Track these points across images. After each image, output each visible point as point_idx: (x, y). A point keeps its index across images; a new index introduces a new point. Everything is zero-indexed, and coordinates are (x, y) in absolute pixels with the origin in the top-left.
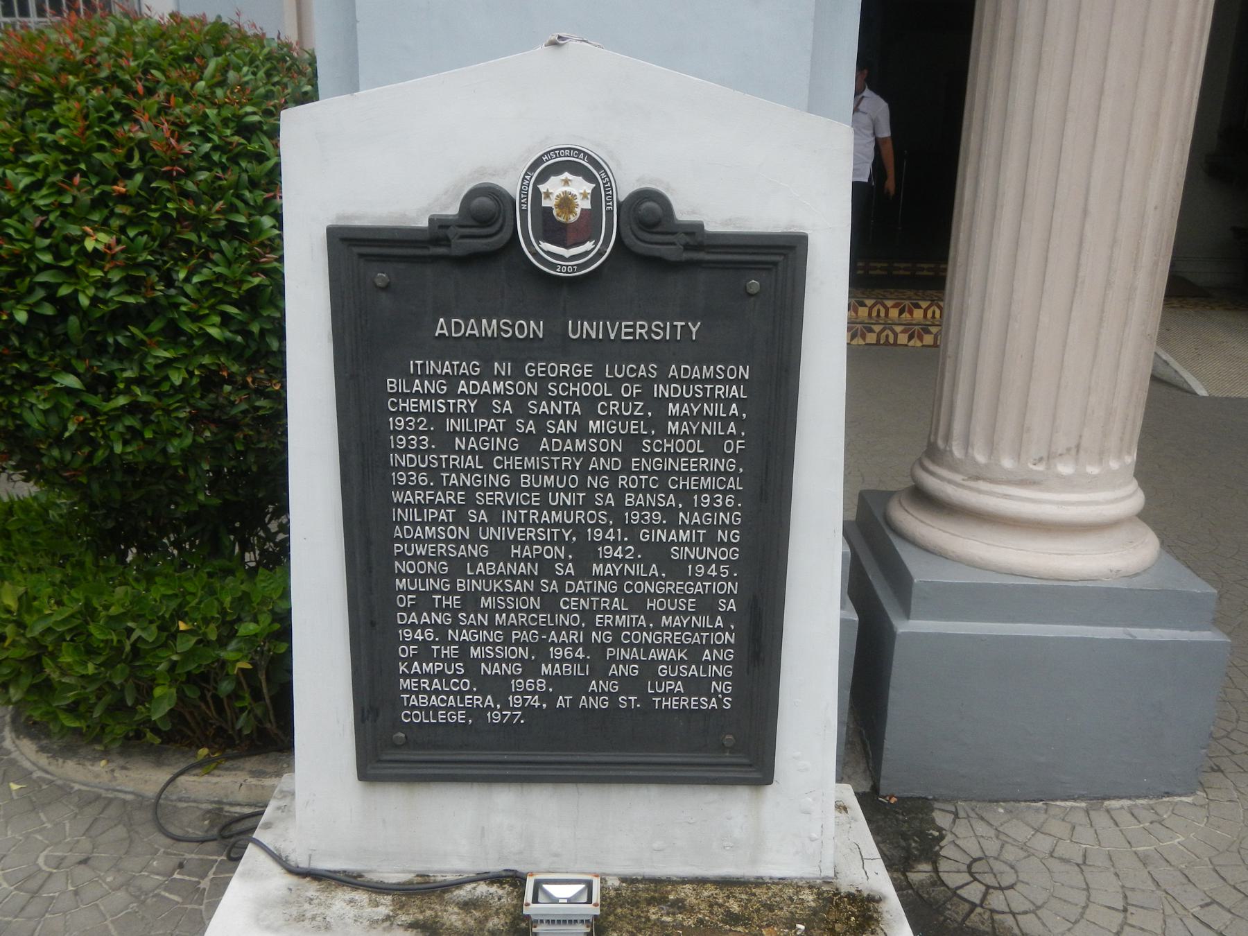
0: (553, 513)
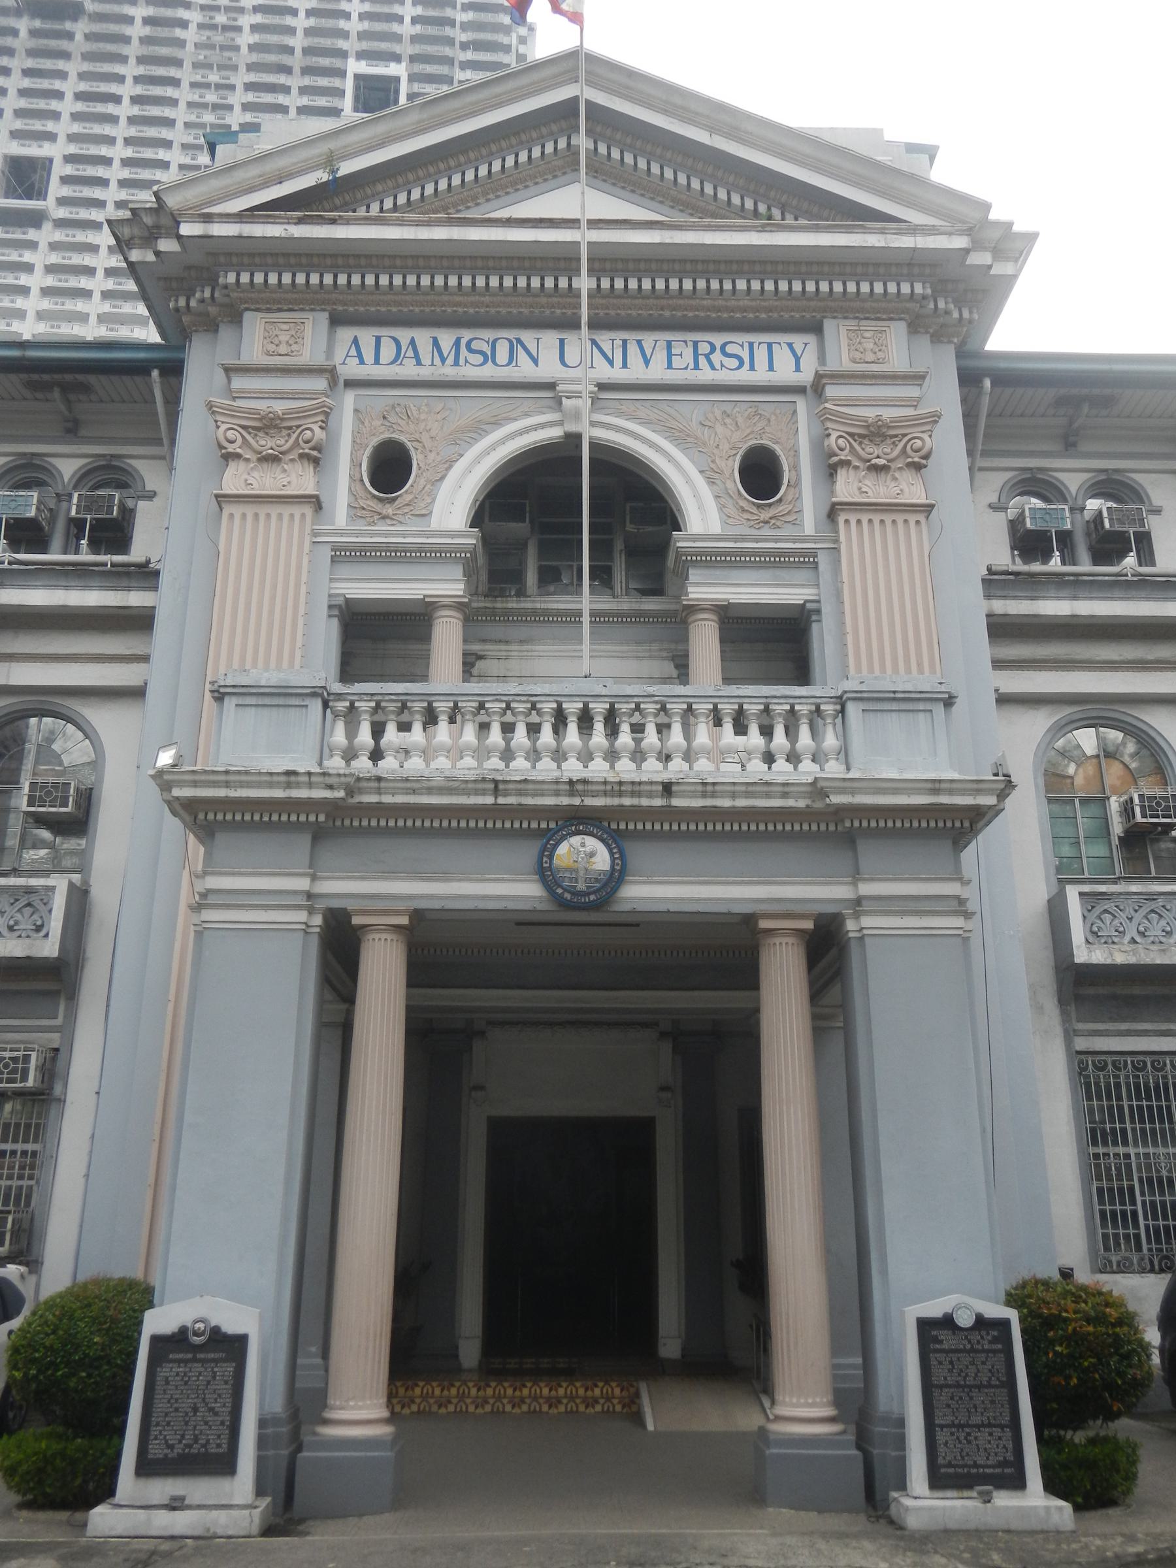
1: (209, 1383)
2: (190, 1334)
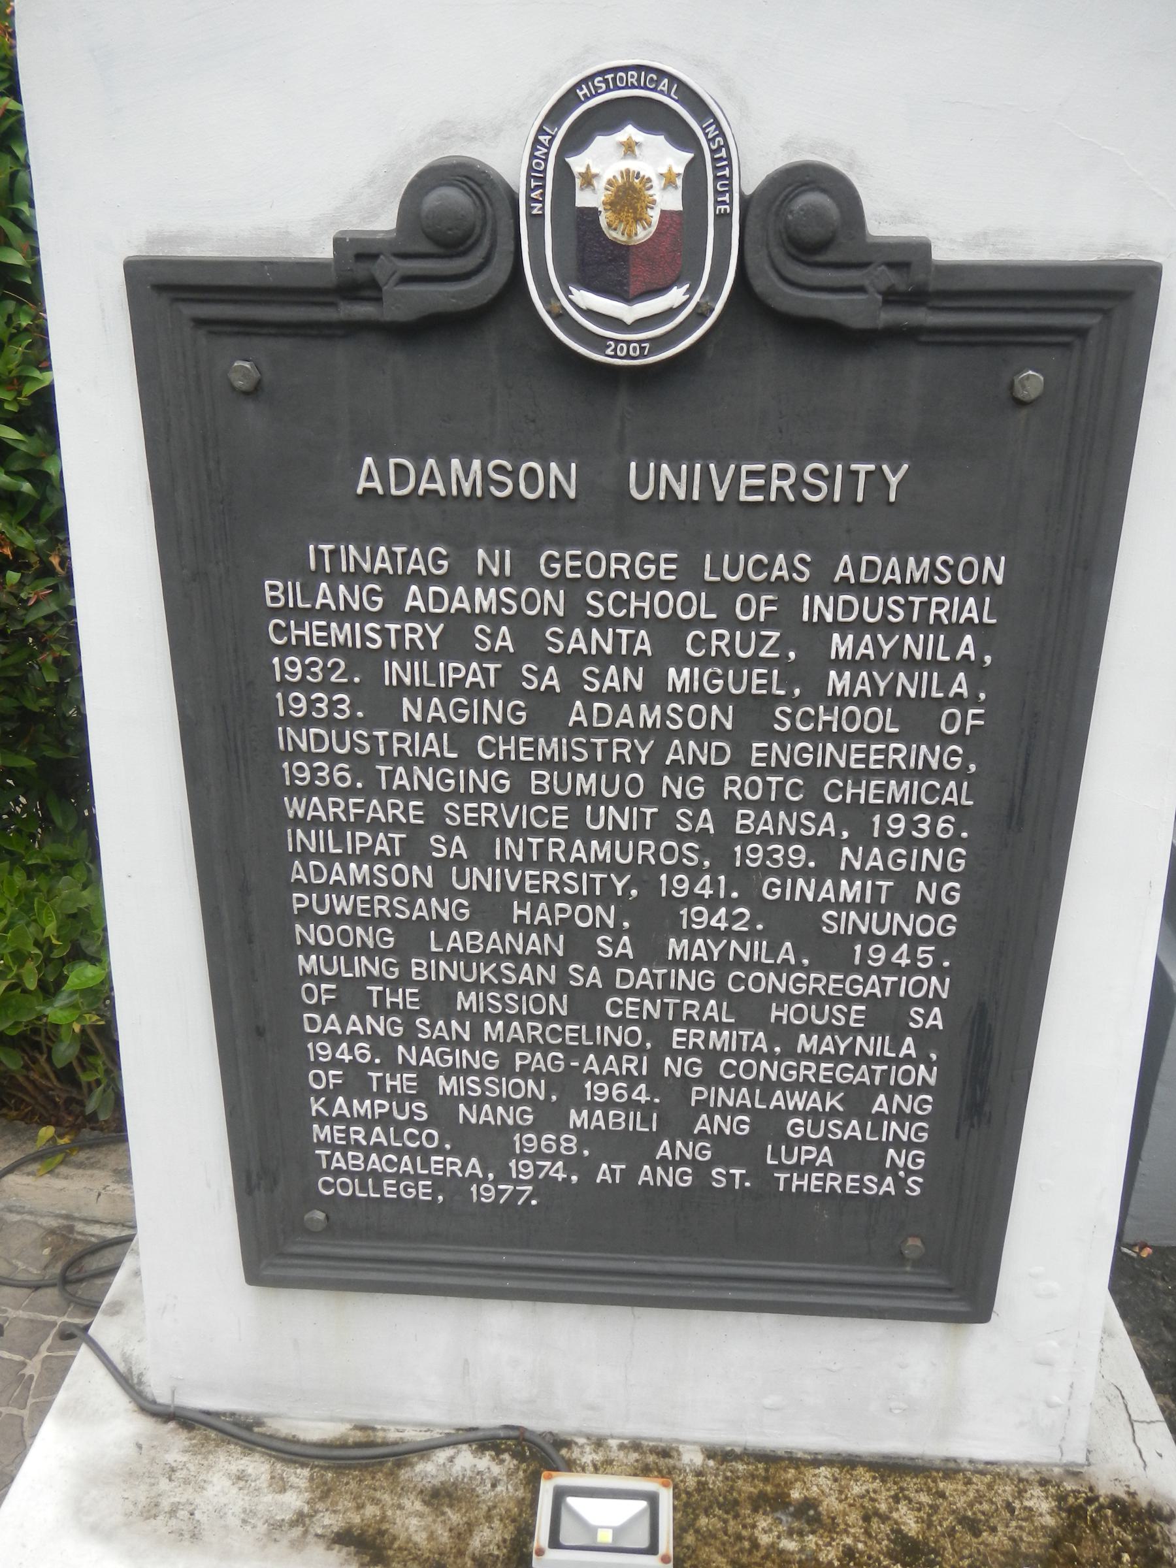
0: (479, 591)
1: (755, 714)
2: (541, 253)
